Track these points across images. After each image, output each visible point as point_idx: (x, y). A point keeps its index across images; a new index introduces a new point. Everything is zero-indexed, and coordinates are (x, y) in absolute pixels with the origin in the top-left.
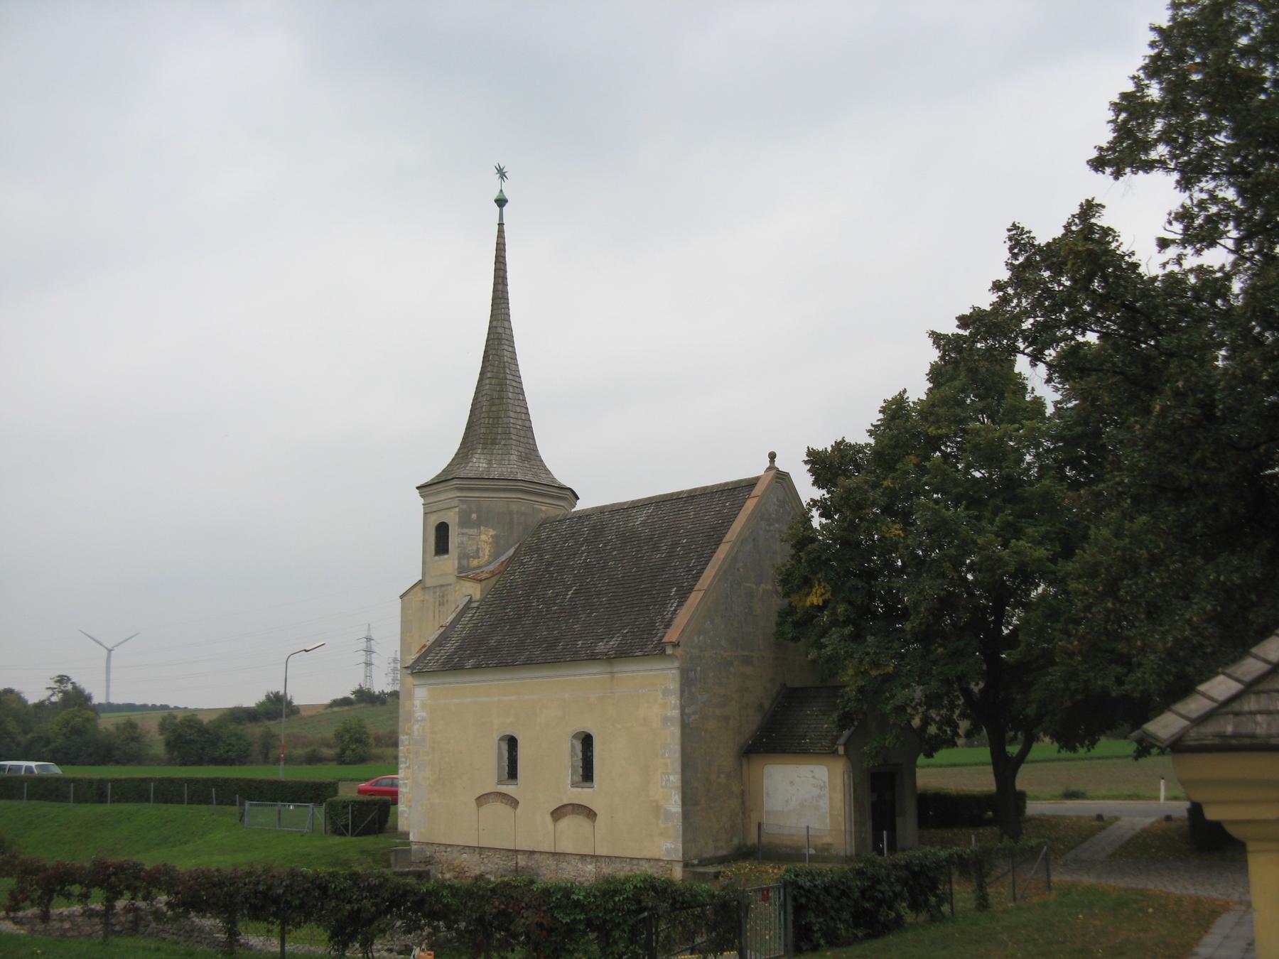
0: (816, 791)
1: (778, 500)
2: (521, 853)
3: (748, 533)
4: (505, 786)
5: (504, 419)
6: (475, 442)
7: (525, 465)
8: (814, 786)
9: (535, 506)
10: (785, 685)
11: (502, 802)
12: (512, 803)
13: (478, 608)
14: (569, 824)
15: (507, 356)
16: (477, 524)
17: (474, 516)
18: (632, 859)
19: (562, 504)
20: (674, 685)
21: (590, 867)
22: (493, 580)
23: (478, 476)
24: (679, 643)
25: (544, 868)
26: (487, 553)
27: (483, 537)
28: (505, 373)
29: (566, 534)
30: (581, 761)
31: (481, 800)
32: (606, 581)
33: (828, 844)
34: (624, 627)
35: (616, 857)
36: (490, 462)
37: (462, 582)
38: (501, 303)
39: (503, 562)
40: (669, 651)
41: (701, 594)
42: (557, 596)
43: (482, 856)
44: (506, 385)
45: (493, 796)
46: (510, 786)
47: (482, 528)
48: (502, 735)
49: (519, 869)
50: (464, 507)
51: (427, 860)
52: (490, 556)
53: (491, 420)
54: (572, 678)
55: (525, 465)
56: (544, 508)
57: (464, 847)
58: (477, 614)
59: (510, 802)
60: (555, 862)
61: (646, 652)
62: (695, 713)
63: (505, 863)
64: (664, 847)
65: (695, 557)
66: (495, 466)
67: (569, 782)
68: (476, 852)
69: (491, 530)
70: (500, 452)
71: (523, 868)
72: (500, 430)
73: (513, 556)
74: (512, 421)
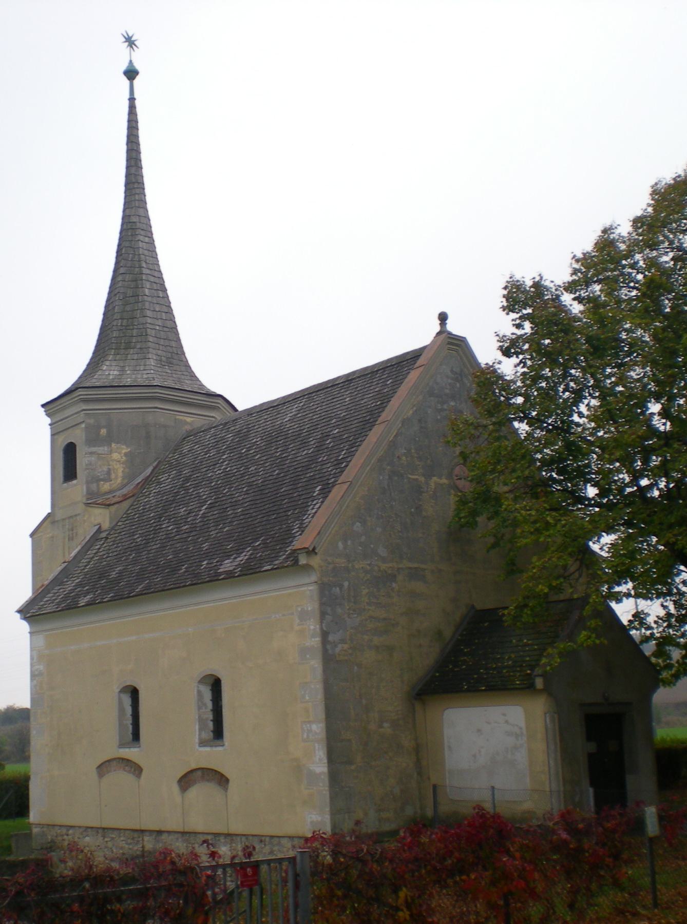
1: (452, 371)
2: (147, 834)
3: (411, 412)
4: (127, 750)
5: (140, 319)
6: (107, 348)
7: (164, 370)
9: (178, 417)
10: (473, 607)
12: (135, 770)
13: (107, 538)
14: (200, 792)
15: (142, 248)
16: (108, 440)
17: (103, 431)
18: (272, 837)
19: (212, 415)
20: (312, 606)
22: (126, 505)
23: (107, 384)
24: (314, 549)
26: (120, 474)
27: (115, 456)
28: (141, 267)
29: (209, 444)
30: (211, 713)
31: (103, 768)
32: (245, 490)
34: (256, 540)
35: (253, 836)
36: (122, 369)
37: (90, 509)
38: (134, 188)
40: (303, 560)
41: (345, 486)
42: (189, 513)
43: (106, 839)
44: (142, 280)
45: (115, 762)
46: (132, 750)
47: (113, 445)
48: (121, 687)
49: (146, 854)
51: (49, 845)
52: (124, 478)
53: (125, 321)
55: (164, 370)
56: (189, 420)
58: (105, 545)
59: (133, 769)
60: (185, 845)
61: (275, 565)
62: (343, 641)
63: (131, 847)
65: (346, 448)
66: (128, 372)
67: (197, 741)
68: (100, 835)
70: (136, 357)
72: (135, 332)
73: (149, 476)
74: (149, 320)
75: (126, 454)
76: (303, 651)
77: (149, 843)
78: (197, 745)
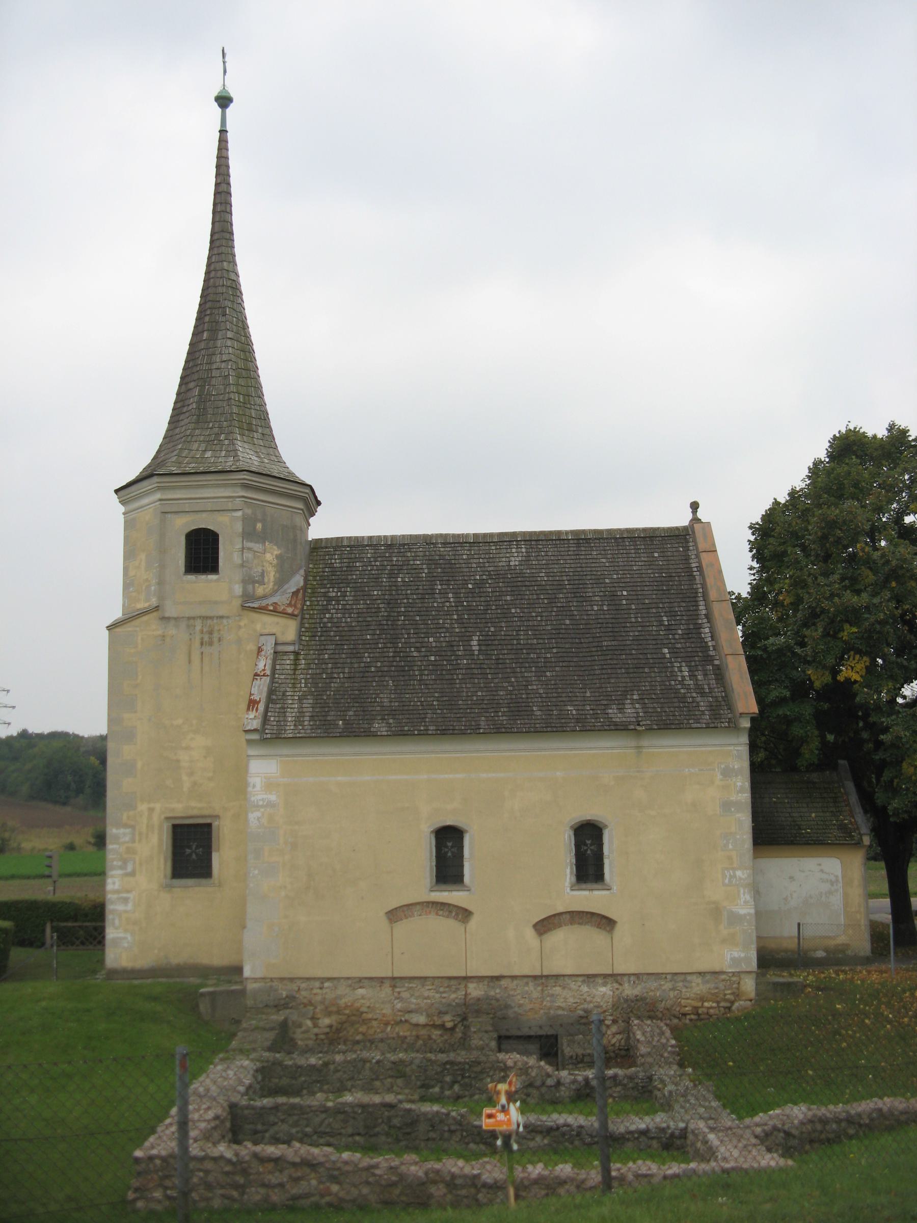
4: (446, 894)
8: (822, 880)
11: (437, 914)
16: (262, 538)
25: (519, 997)
26: (272, 579)
27: (269, 556)
33: (843, 944)
39: (295, 594)
45: (418, 907)
46: (455, 893)
50: (249, 511)
51: (282, 1002)
54: (698, 749)
57: (360, 980)
60: (540, 988)
69: (275, 547)
71: (479, 999)
75: (277, 557)
76: (727, 806)
77: (475, 991)
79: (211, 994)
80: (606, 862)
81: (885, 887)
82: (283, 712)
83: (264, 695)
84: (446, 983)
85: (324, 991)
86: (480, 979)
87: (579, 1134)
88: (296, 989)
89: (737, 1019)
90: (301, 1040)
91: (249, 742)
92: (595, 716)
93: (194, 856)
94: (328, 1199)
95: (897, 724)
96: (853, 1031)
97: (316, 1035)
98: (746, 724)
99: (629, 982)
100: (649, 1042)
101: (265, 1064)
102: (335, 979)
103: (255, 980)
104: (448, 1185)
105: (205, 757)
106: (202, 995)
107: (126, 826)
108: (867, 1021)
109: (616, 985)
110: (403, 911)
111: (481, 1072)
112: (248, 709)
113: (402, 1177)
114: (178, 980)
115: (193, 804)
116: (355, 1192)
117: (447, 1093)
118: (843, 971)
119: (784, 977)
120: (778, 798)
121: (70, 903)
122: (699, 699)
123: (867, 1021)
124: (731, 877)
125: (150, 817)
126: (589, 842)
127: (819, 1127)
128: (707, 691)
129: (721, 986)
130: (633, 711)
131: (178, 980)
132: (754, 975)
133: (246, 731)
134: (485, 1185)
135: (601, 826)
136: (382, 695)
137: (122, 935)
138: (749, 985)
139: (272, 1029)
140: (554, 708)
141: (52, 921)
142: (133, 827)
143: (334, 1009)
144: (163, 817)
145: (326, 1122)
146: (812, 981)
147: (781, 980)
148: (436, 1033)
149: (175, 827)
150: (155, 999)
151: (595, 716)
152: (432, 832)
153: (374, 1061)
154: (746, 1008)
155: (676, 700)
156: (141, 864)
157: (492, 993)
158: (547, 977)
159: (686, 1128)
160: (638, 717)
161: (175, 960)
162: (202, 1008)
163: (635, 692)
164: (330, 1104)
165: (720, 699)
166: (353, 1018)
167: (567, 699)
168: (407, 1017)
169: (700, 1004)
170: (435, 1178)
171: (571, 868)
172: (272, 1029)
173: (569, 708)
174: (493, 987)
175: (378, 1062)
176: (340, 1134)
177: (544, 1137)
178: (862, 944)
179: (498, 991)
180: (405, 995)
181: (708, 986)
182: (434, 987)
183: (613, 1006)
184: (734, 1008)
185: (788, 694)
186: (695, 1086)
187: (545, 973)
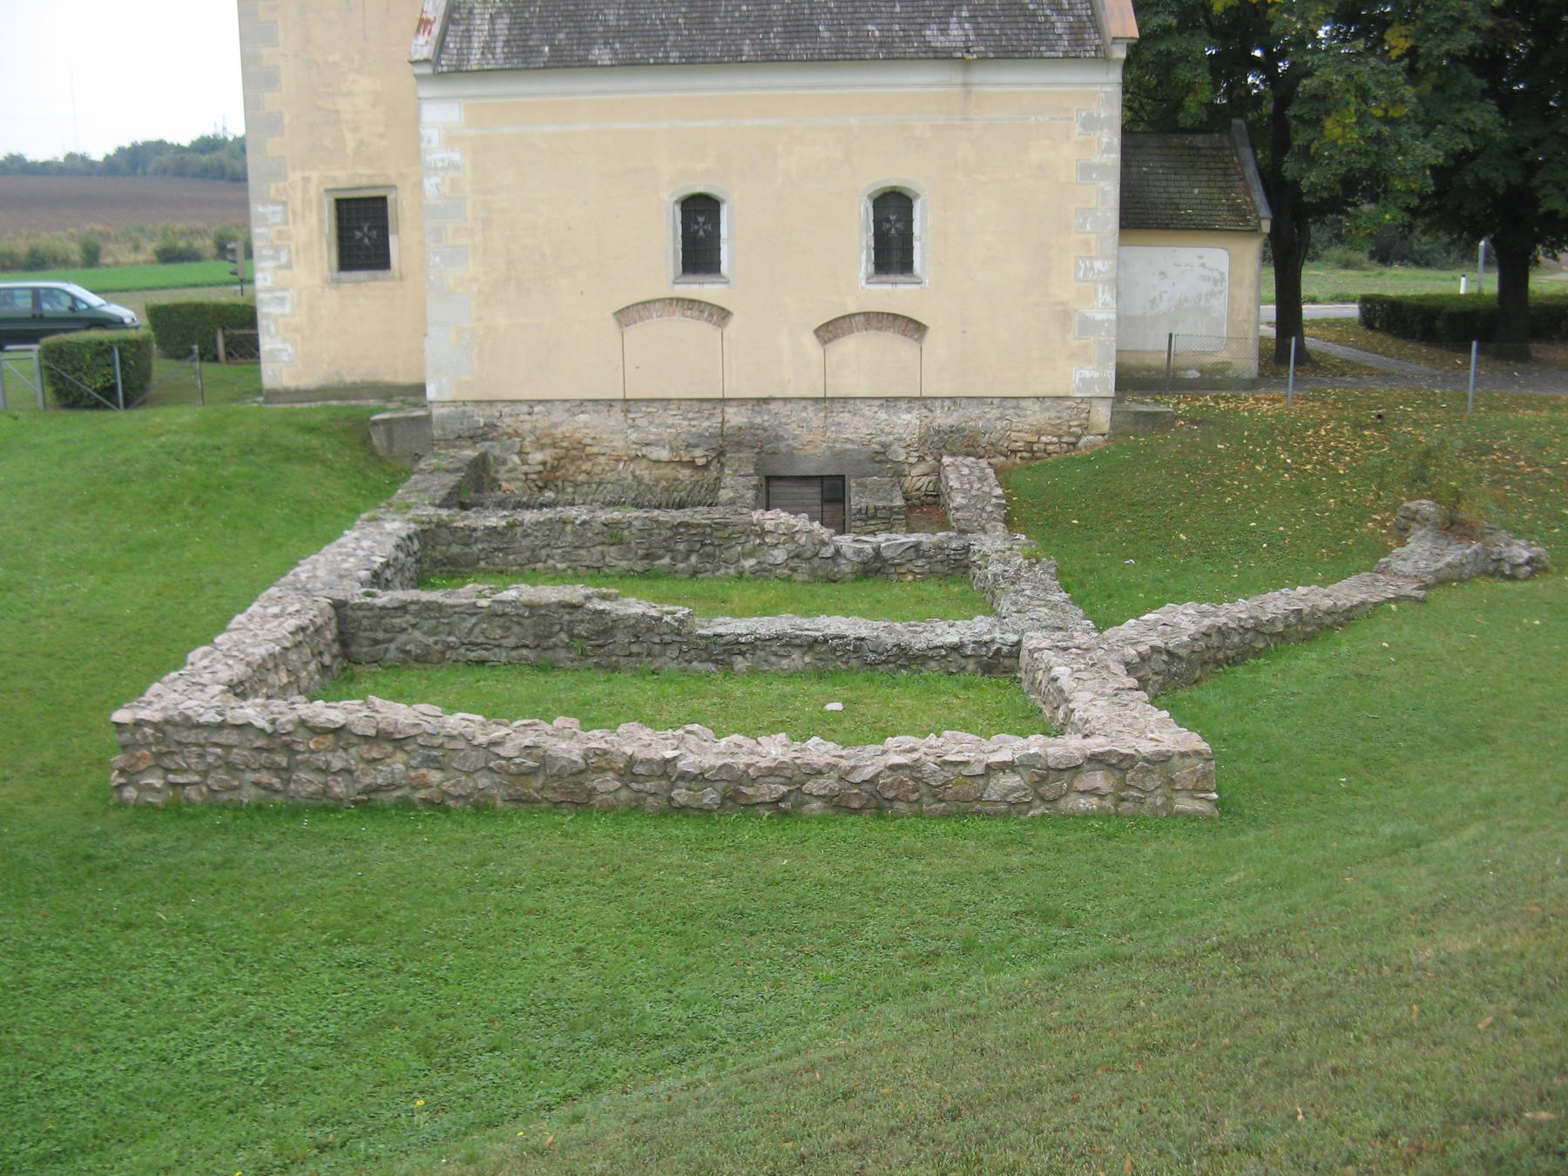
0: (1206, 287)
4: (695, 287)
8: (1203, 278)
21: (907, 417)
25: (794, 426)
45: (658, 305)
51: (480, 432)
57: (582, 402)
60: (822, 414)
64: (1078, 376)
71: (740, 428)
76: (1086, 170)
77: (736, 417)
78: (863, 283)
79: (385, 421)
80: (917, 245)
81: (1270, 291)
82: (467, 36)
83: (442, 11)
84: (696, 406)
85: (534, 417)
86: (742, 401)
87: (857, 649)
88: (498, 414)
89: (1085, 461)
90: (506, 481)
91: (419, 77)
92: (907, 39)
93: (366, 241)
94: (423, 794)
95: (1326, 65)
96: (1240, 481)
97: (526, 474)
98: (1120, 53)
99: (943, 407)
100: (965, 491)
101: (426, 527)
102: (548, 401)
103: (443, 403)
104: (620, 775)
105: (373, 106)
106: (375, 423)
107: (274, 202)
108: (1258, 467)
109: (925, 412)
110: (638, 311)
111: (729, 538)
112: (418, 31)
113: (545, 761)
114: (353, 402)
115: (361, 170)
116: (467, 784)
117: (681, 566)
118: (1223, 398)
119: (1147, 405)
120: (1148, 167)
121: (244, 306)
122: (1054, 18)
123: (1258, 467)
124: (1087, 269)
125: (305, 190)
126: (893, 218)
127: (1215, 641)
128: (1067, 7)
129: (1065, 414)
130: (961, 32)
131: (353, 402)
132: (1110, 402)
133: (414, 63)
134: (683, 776)
135: (910, 195)
136: (606, 11)
137: (280, 346)
138: (1102, 416)
139: (458, 470)
140: (849, 28)
141: (224, 328)
142: (284, 204)
143: (547, 441)
144: (322, 189)
145: (477, 630)
146: (1186, 411)
147: (1145, 409)
148: (684, 473)
149: (339, 202)
150: (311, 430)
151: (907, 39)
152: (676, 202)
153: (578, 522)
154: (1096, 445)
155: (1021, 19)
156: (297, 253)
157: (758, 420)
158: (832, 399)
159: (1019, 642)
160: (967, 41)
161: (349, 378)
162: (375, 441)
163: (965, 8)
164: (484, 603)
165: (1085, 19)
166: (574, 453)
167: (868, 15)
168: (645, 451)
169: (1035, 439)
170: (599, 762)
171: (868, 254)
172: (458, 470)
173: (870, 28)
174: (759, 413)
175: (584, 523)
176: (499, 646)
177: (805, 654)
178: (1247, 362)
179: (766, 417)
180: (642, 422)
181: (1047, 415)
182: (680, 412)
183: (920, 439)
184: (1080, 444)
185: (1173, 21)
186: (1031, 565)
187: (829, 395)
